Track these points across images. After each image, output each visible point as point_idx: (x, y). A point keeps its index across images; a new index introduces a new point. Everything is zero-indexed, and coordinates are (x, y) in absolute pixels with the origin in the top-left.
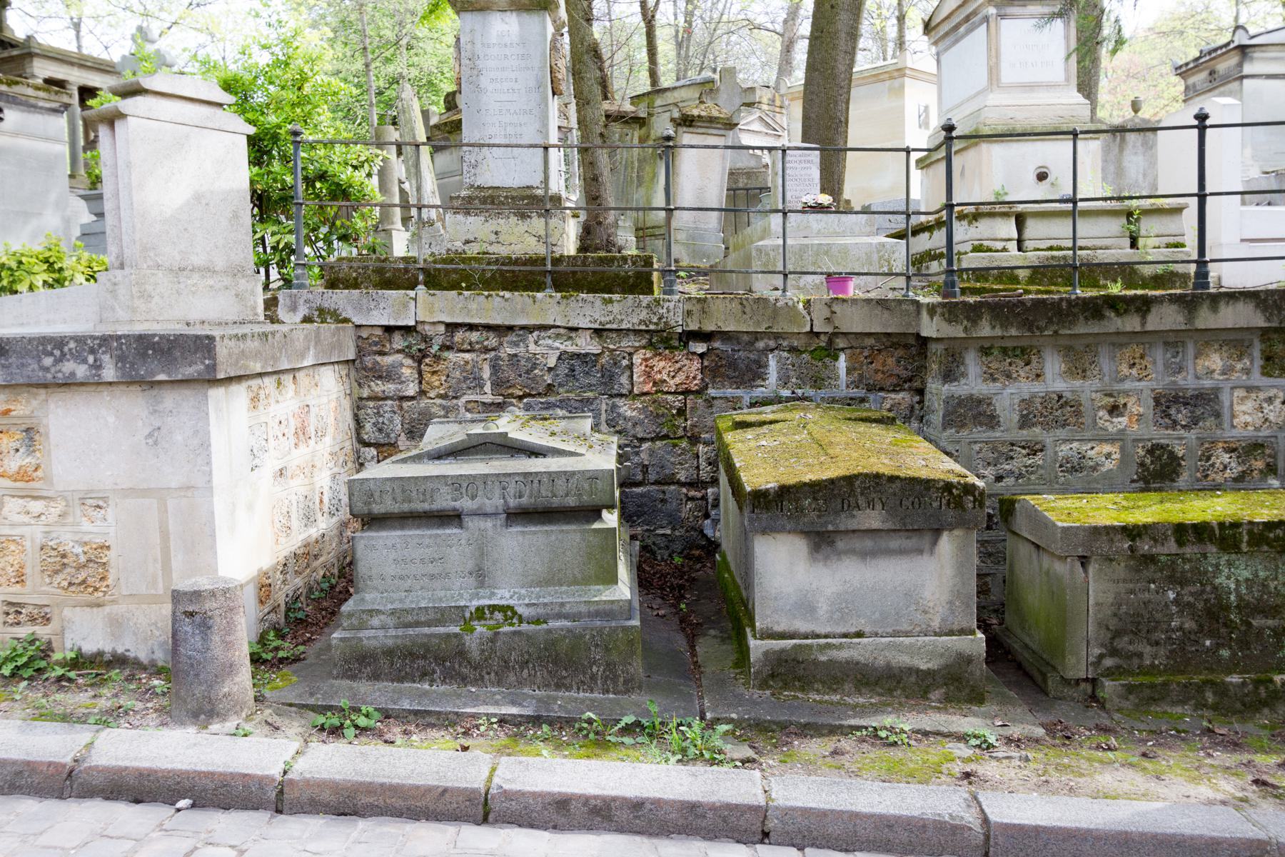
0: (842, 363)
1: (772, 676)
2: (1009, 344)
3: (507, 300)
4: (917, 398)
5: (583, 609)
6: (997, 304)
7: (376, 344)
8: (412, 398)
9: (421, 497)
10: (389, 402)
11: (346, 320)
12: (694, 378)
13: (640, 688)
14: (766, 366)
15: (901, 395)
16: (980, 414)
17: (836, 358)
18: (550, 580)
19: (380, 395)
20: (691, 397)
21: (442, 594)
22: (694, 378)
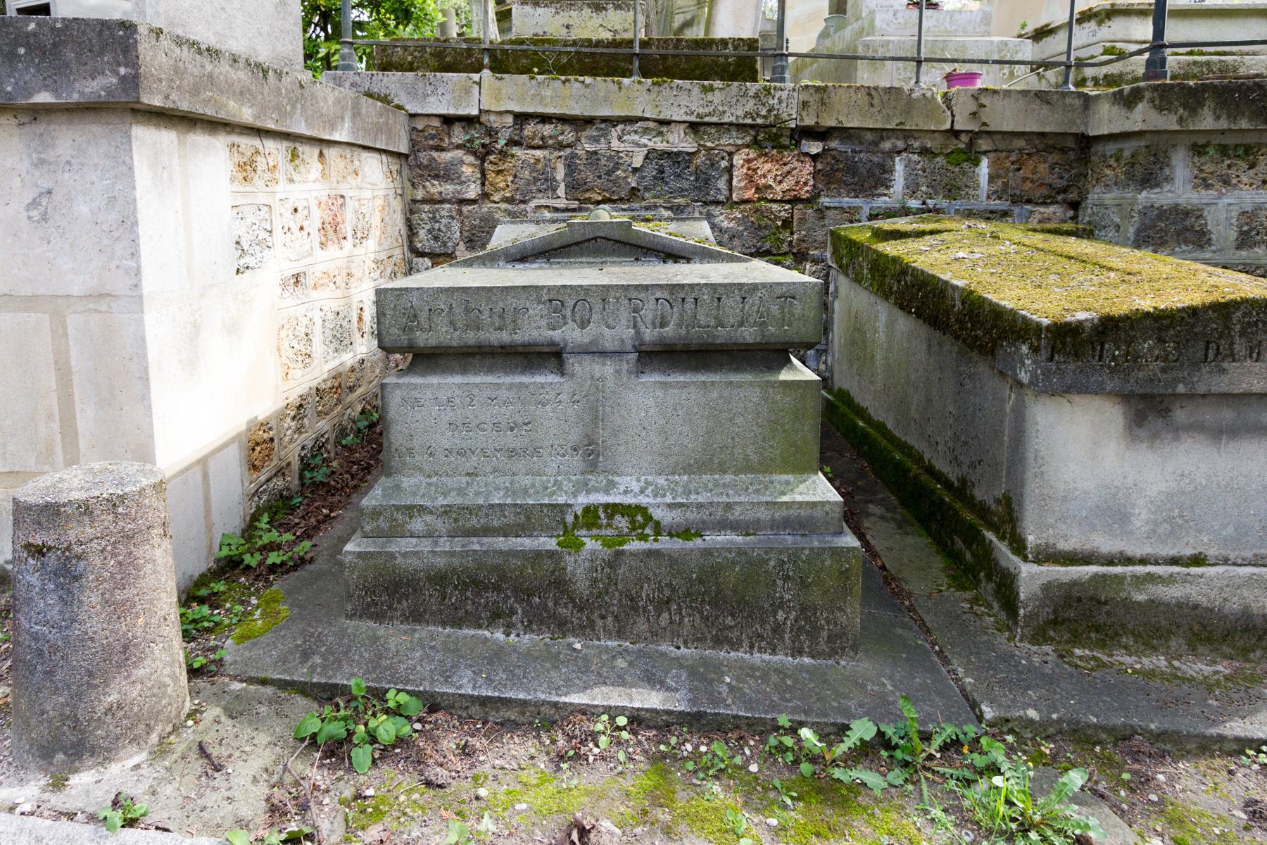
0: (984, 168)
1: (1055, 623)
2: (1230, 140)
3: (587, 86)
4: (1071, 213)
5: (764, 514)
6: (1225, 87)
7: (433, 137)
8: (473, 201)
9: (497, 323)
10: (447, 206)
11: (399, 107)
12: (805, 184)
13: (855, 648)
14: (891, 171)
15: (1052, 209)
16: (1187, 229)
17: (977, 163)
18: (703, 463)
19: (437, 197)
20: (800, 206)
21: (527, 481)
22: (805, 184)
